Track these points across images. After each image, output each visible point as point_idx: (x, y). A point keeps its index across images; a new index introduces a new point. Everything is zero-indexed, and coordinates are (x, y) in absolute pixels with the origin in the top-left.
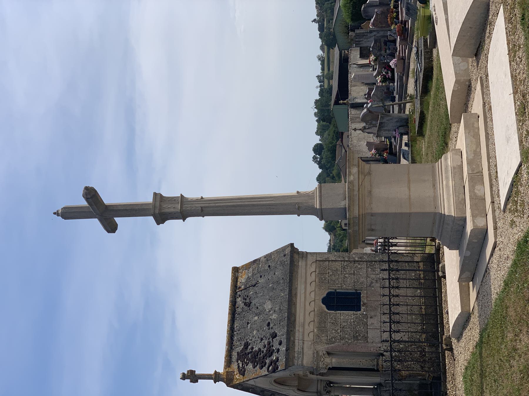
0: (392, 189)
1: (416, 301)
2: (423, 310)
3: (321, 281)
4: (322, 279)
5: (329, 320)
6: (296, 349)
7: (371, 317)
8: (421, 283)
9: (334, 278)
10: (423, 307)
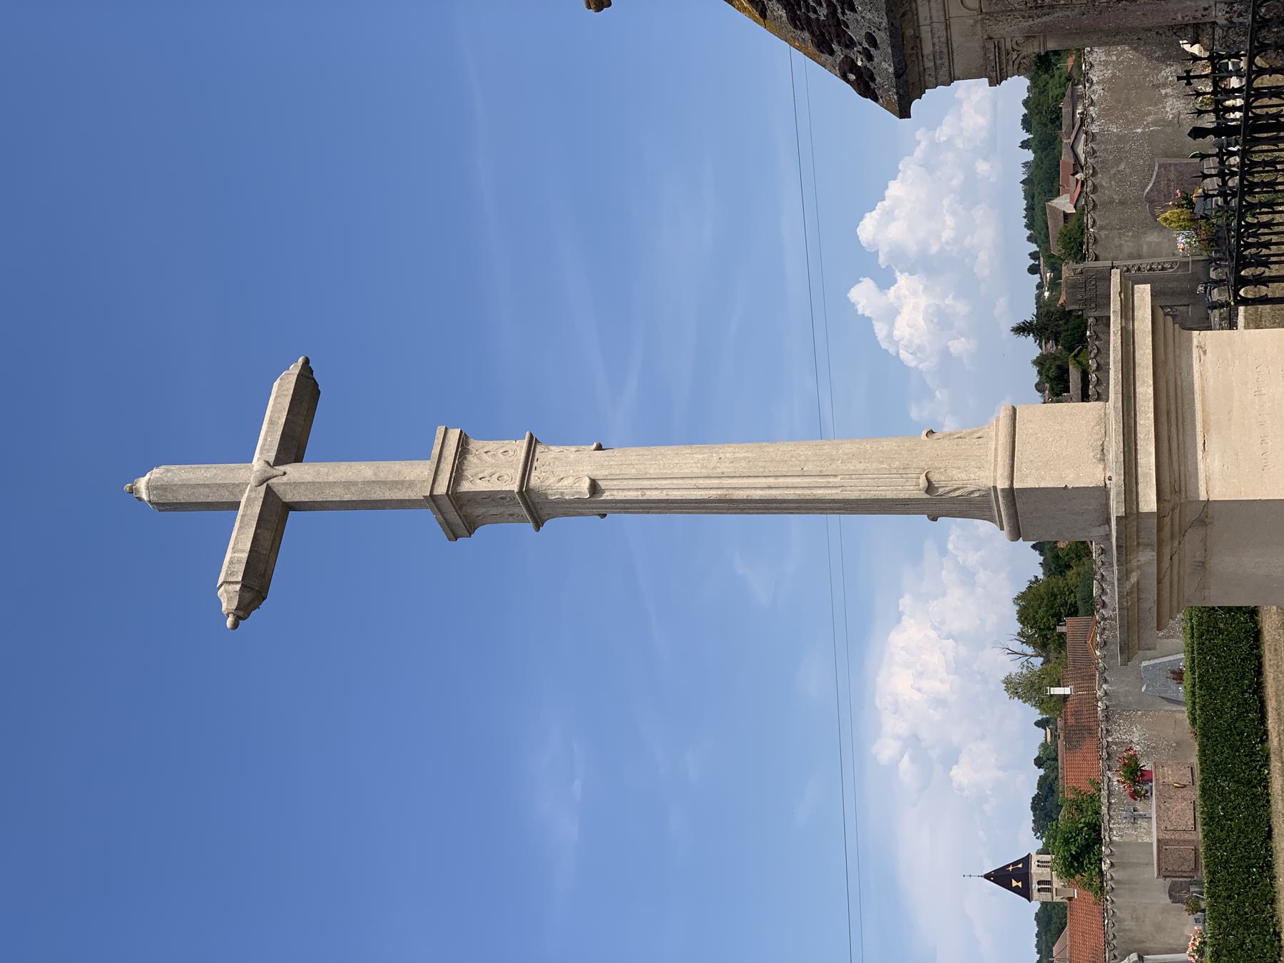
6: (927, 49)
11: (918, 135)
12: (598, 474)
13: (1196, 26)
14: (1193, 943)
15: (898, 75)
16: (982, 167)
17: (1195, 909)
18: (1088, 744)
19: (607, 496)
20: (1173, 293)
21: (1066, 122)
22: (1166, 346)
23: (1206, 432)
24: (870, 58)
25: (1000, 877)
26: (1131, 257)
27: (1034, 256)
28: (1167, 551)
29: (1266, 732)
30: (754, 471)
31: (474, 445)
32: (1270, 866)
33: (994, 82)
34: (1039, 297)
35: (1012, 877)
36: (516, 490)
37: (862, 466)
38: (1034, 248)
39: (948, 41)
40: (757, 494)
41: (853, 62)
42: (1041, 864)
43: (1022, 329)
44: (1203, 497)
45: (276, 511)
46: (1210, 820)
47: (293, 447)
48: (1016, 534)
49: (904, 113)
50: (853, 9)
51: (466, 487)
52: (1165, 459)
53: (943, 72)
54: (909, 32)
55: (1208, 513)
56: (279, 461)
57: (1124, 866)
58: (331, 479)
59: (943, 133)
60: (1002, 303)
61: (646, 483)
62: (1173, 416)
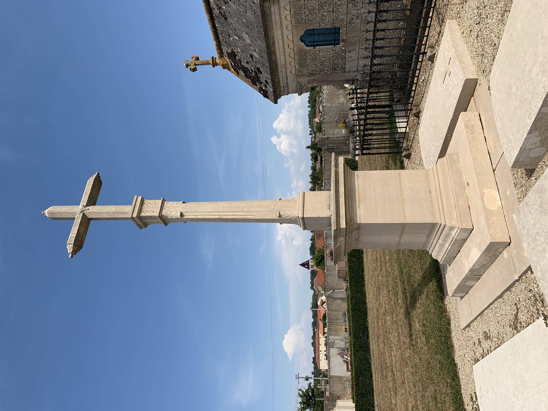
0: (382, 197)
1: (396, 34)
2: (402, 42)
3: (298, 21)
4: (298, 19)
5: (309, 57)
6: (282, 85)
7: (349, 52)
8: (406, 15)
9: (311, 18)
10: (403, 39)
11: (286, 104)
12: (182, 211)
13: (353, 80)
14: (345, 288)
15: (274, 92)
16: (300, 111)
17: (345, 280)
18: (321, 238)
19: (185, 217)
20: (341, 143)
21: (317, 102)
24: (266, 87)
25: (303, 265)
26: (332, 135)
27: (310, 131)
28: (348, 237)
30: (230, 210)
31: (146, 201)
32: (363, 278)
33: (300, 94)
34: (312, 140)
35: (305, 265)
36: (158, 215)
37: (260, 209)
38: (310, 129)
39: (287, 83)
40: (230, 217)
41: (262, 88)
42: (311, 262)
43: (308, 147)
44: (359, 222)
45: (86, 221)
46: (350, 267)
47: (92, 201)
48: (305, 228)
49: (276, 102)
50: (261, 73)
51: (143, 214)
52: (348, 211)
53: (286, 91)
54: (277, 80)
55: (359, 227)
56: (87, 205)
57: (330, 271)
58: (102, 211)
59: (291, 104)
60: (303, 142)
61: (197, 214)
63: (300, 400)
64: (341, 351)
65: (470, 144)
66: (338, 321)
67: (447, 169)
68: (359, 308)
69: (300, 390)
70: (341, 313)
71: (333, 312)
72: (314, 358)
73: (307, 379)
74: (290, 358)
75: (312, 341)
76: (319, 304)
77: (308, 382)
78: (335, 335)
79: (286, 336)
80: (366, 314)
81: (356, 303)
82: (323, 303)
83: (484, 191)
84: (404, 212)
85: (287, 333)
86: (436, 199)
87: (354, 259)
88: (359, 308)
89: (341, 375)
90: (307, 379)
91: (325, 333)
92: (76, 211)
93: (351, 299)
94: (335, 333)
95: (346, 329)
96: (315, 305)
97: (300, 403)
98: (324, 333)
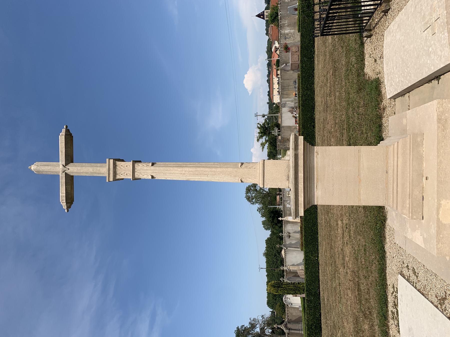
22: (307, 154)
23: (317, 182)
25: (259, 16)
29: (314, 46)
32: (313, 76)
44: (316, 204)
47: (69, 159)
56: (67, 164)
62: (308, 178)
63: (258, 130)
64: (292, 109)
65: (438, 143)
66: (289, 87)
67: (408, 151)
68: (308, 103)
69: (258, 124)
70: (292, 81)
71: (285, 81)
72: (269, 92)
73: (264, 116)
74: (250, 93)
75: (267, 79)
76: (273, 50)
77: (265, 118)
78: (286, 98)
79: (246, 76)
80: (314, 108)
81: (306, 100)
82: (276, 49)
83: (442, 202)
84: (359, 194)
85: (247, 73)
86: (392, 181)
87: (306, 59)
88: (308, 103)
89: (290, 125)
90: (264, 116)
91: (278, 75)
92: (58, 168)
93: (302, 96)
94: (287, 96)
95: (296, 94)
96: (269, 52)
97: (259, 133)
98: (277, 75)
